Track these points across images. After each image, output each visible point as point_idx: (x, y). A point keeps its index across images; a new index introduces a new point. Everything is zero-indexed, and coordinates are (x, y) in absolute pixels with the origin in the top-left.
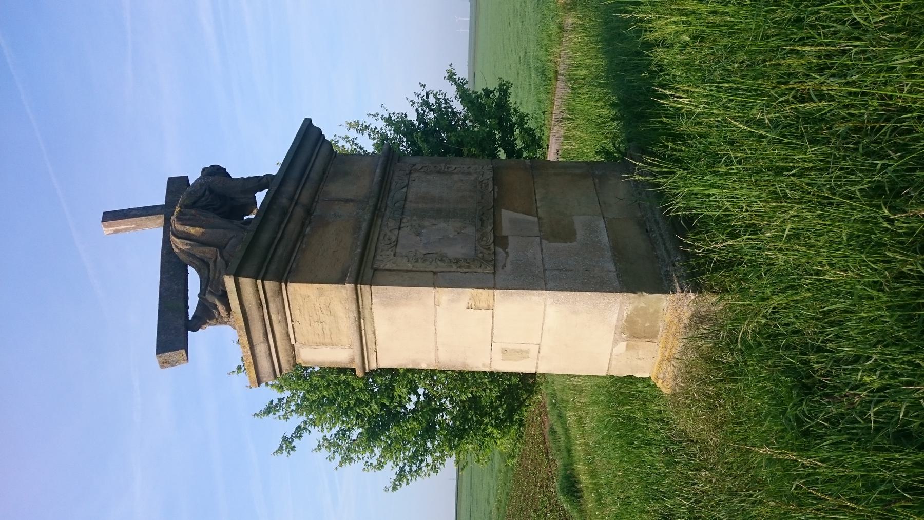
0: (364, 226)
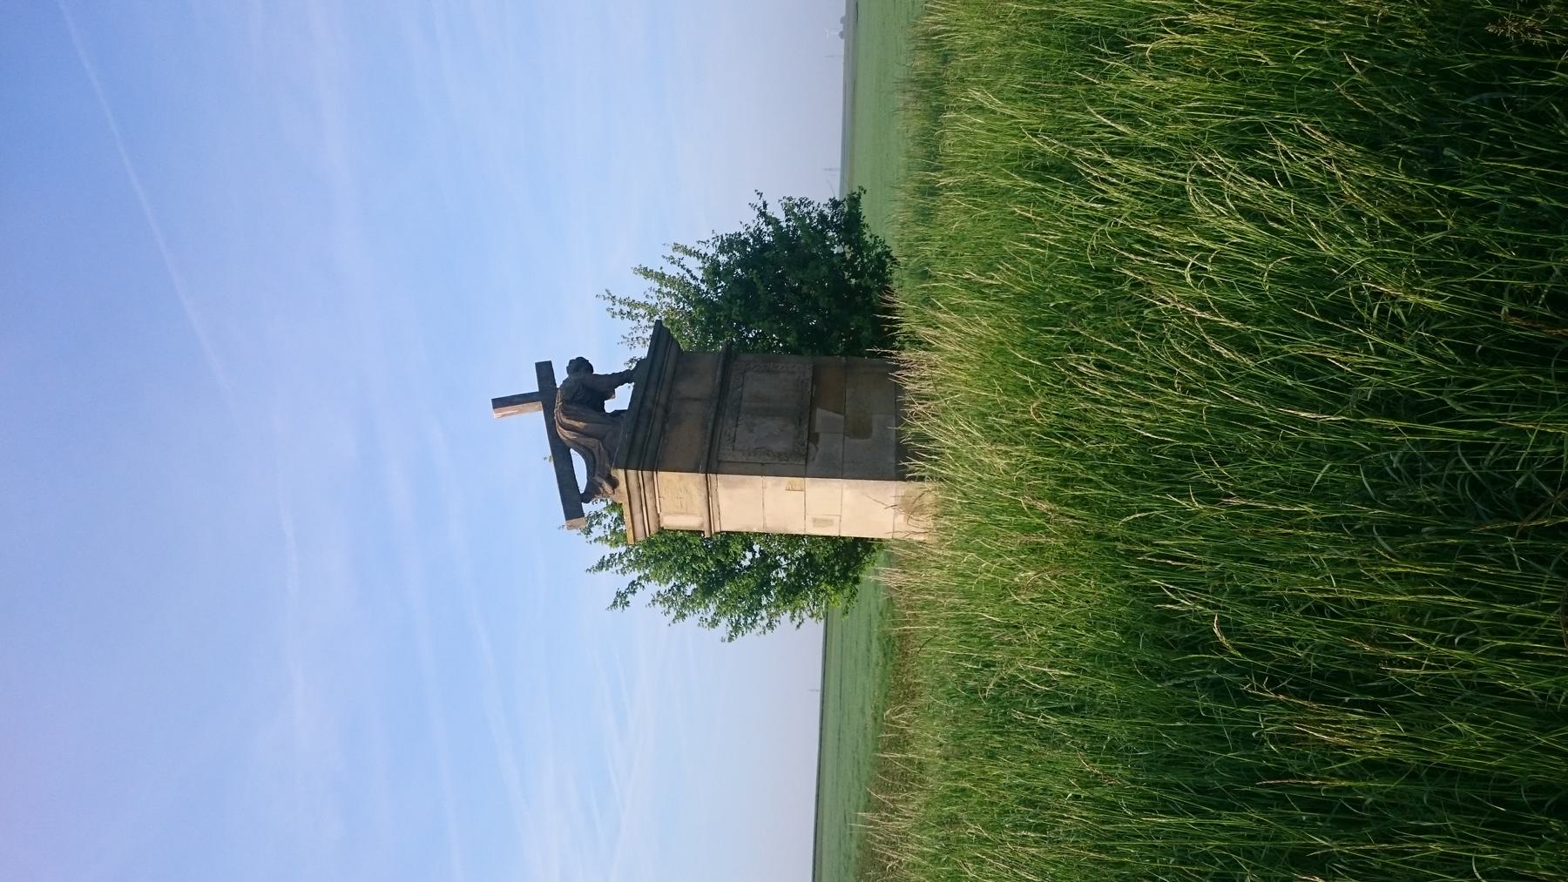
0: (710, 425)
